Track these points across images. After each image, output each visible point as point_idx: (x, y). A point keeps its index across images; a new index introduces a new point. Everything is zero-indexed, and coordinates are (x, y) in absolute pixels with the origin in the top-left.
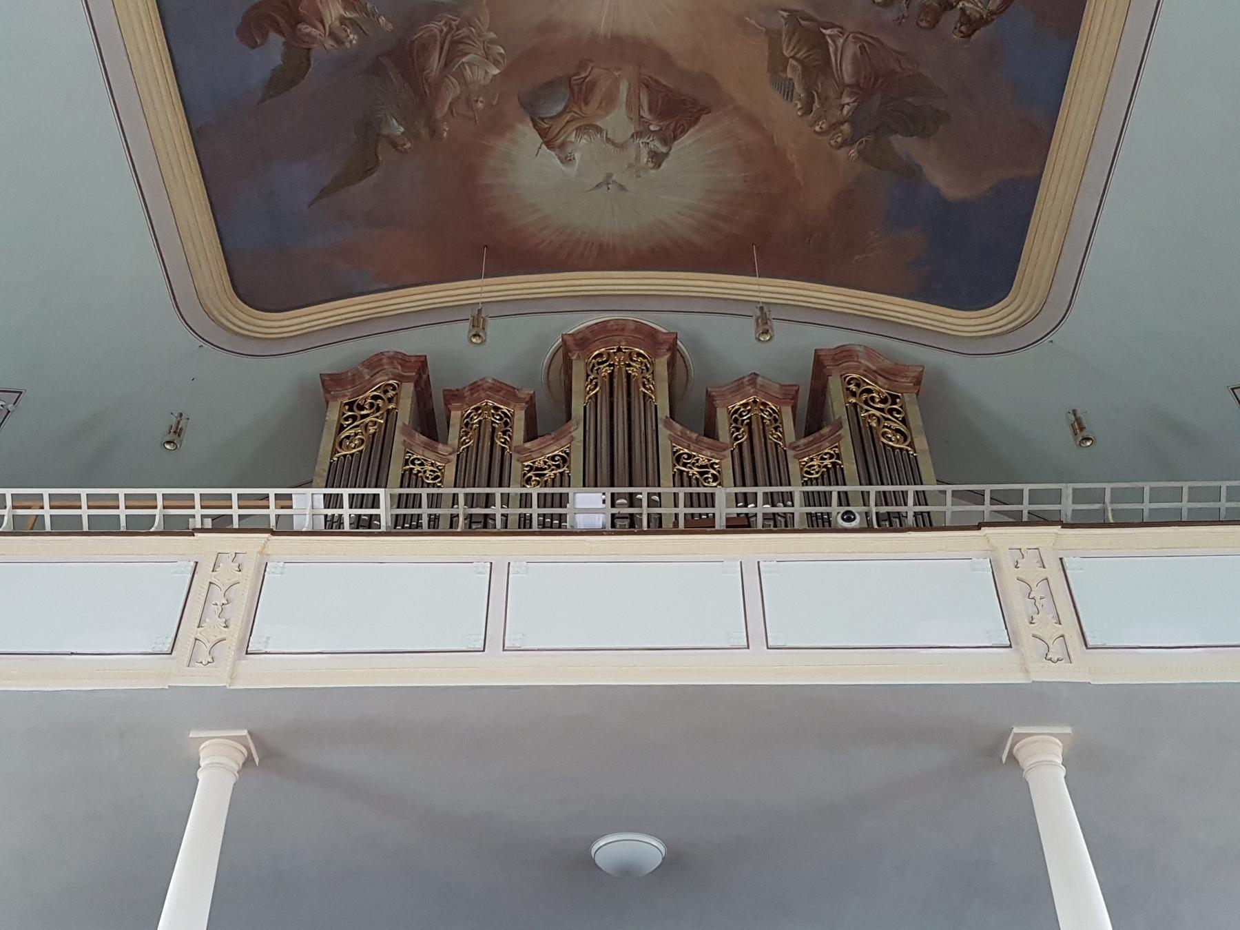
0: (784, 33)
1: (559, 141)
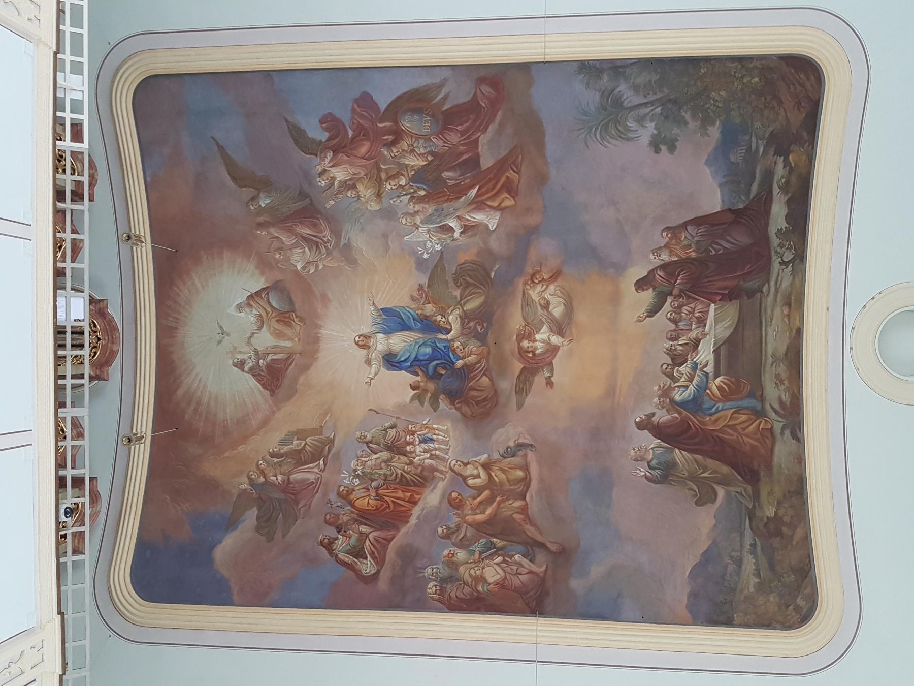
0: (321, 437)
1: (252, 303)
